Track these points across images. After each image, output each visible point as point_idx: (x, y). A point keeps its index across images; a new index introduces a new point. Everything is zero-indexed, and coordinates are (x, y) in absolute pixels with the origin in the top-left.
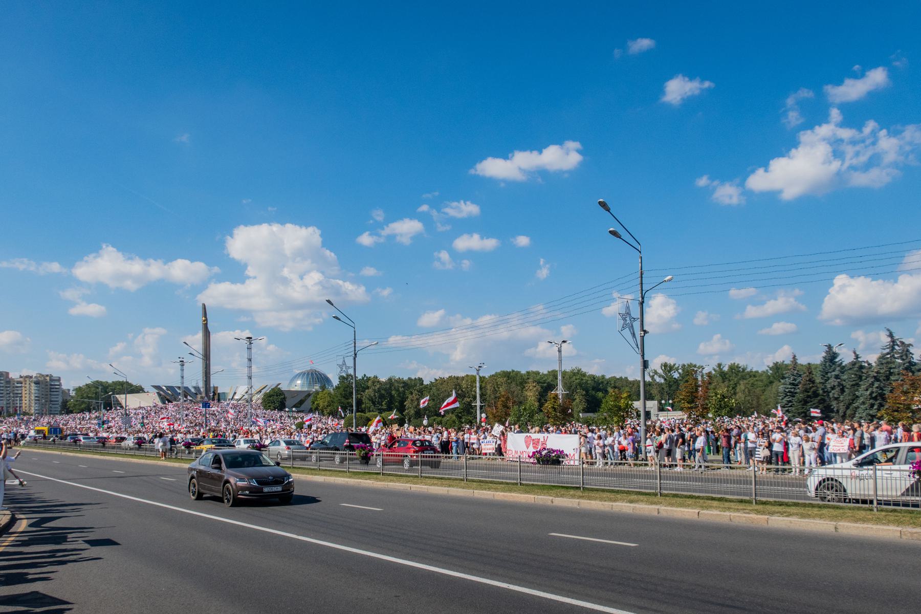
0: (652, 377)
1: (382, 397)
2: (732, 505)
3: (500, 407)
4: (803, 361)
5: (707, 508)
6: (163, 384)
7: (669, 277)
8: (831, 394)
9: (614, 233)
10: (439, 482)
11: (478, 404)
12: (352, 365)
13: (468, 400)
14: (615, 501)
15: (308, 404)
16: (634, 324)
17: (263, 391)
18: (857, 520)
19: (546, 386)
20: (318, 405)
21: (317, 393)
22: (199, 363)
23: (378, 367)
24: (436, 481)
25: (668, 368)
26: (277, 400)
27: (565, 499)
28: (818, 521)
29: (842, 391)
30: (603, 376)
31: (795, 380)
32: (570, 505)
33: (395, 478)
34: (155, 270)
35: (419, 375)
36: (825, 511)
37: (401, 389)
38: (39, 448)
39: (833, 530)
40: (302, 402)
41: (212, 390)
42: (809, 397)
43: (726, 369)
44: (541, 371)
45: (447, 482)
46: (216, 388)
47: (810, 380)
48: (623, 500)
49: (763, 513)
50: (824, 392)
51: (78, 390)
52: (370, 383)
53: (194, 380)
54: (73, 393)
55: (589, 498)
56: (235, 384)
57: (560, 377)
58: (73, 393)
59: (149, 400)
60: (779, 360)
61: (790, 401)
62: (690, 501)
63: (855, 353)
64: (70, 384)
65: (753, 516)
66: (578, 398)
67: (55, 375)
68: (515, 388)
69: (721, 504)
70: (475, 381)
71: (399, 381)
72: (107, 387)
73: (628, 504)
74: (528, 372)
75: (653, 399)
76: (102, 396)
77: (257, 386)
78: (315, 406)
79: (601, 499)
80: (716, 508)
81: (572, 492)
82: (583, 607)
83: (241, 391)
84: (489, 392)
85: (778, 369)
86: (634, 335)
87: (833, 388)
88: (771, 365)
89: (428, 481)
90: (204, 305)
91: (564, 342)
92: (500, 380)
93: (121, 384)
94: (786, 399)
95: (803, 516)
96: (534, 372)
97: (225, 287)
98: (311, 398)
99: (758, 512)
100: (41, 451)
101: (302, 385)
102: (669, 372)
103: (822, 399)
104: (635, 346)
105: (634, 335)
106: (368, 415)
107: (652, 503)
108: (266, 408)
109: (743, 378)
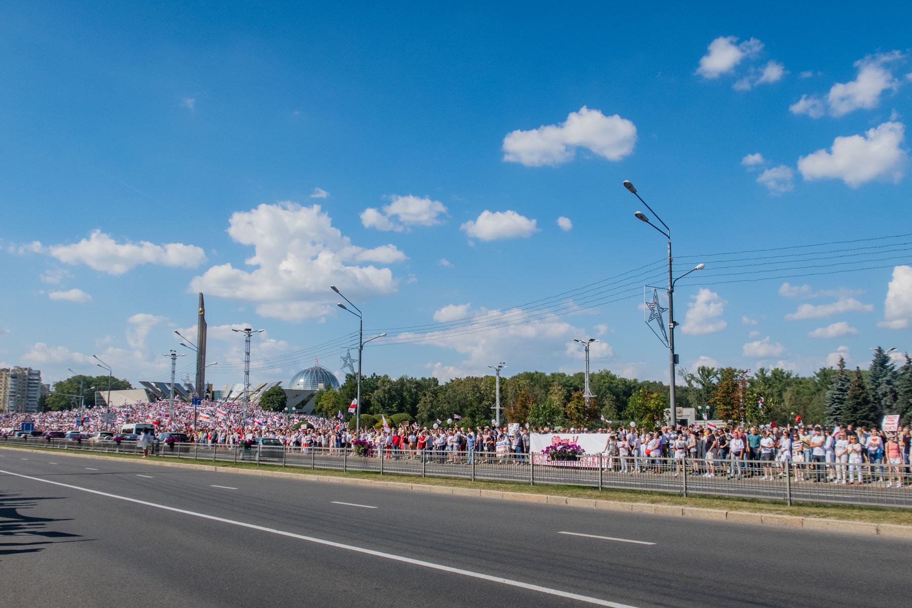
0: (689, 382)
1: (392, 398)
2: (764, 506)
3: (518, 406)
4: (850, 367)
5: (736, 508)
6: (152, 379)
7: (700, 265)
8: (883, 402)
9: (641, 217)
10: (444, 481)
11: (498, 407)
12: (358, 358)
13: (487, 403)
14: (636, 501)
15: (311, 405)
16: (663, 315)
17: (262, 390)
18: (900, 522)
19: (572, 387)
20: (322, 406)
21: (321, 393)
22: (194, 356)
23: (390, 364)
24: (440, 481)
25: (706, 372)
26: (276, 400)
27: (581, 499)
28: (857, 522)
29: (895, 398)
30: (635, 380)
31: (843, 385)
32: (586, 506)
33: (395, 478)
34: (148, 252)
35: (434, 375)
36: (865, 512)
37: (414, 390)
38: (8, 445)
39: (875, 532)
40: (305, 403)
41: (206, 388)
42: (858, 404)
43: (769, 374)
44: (567, 374)
45: (453, 481)
46: (210, 386)
47: (859, 386)
48: (644, 500)
49: (798, 514)
50: (876, 399)
51: (59, 385)
52: (379, 383)
53: (186, 375)
54: (52, 389)
55: (607, 498)
56: (232, 379)
57: (587, 380)
58: (52, 389)
59: (136, 397)
60: (828, 367)
61: (838, 409)
62: (718, 502)
63: (907, 357)
64: (50, 379)
65: (787, 517)
66: (608, 403)
67: (35, 369)
68: (537, 390)
69: (752, 505)
70: (494, 383)
71: (411, 381)
72: (91, 383)
73: (650, 505)
74: (553, 375)
75: (690, 406)
76: (86, 392)
77: (256, 383)
78: (318, 407)
79: (620, 499)
80: (746, 509)
81: (589, 492)
82: (584, 602)
83: (239, 388)
84: (510, 395)
85: (825, 374)
86: (662, 326)
87: (885, 395)
88: (818, 371)
89: (433, 480)
90: (202, 295)
91: (592, 340)
92: (523, 382)
93: (106, 379)
94: (834, 406)
95: (841, 517)
96: (559, 375)
97: (223, 271)
98: (315, 398)
99: (792, 513)
100: (10, 448)
101: (305, 384)
102: (707, 377)
103: (873, 407)
104: (663, 339)
105: (662, 326)
106: (375, 416)
107: (676, 504)
108: (265, 408)
109: (788, 384)
